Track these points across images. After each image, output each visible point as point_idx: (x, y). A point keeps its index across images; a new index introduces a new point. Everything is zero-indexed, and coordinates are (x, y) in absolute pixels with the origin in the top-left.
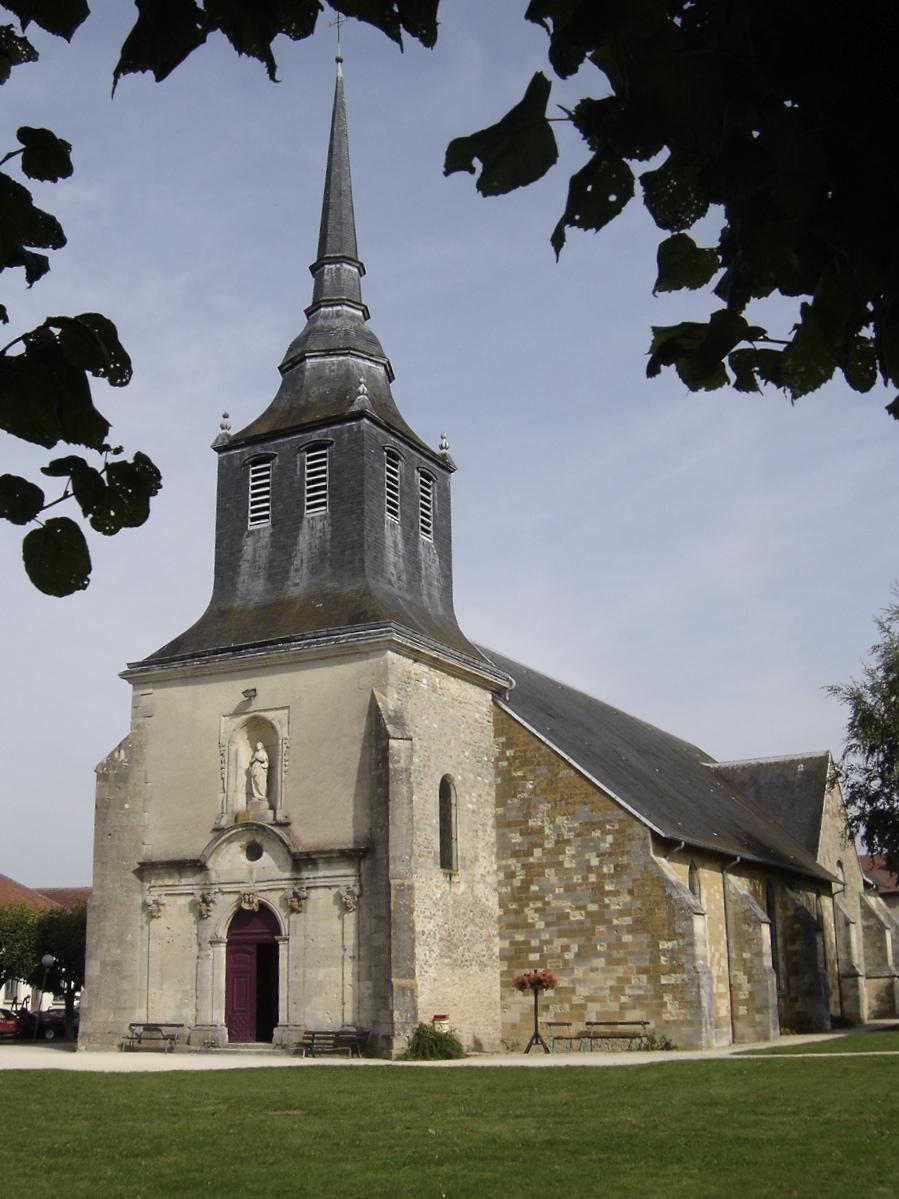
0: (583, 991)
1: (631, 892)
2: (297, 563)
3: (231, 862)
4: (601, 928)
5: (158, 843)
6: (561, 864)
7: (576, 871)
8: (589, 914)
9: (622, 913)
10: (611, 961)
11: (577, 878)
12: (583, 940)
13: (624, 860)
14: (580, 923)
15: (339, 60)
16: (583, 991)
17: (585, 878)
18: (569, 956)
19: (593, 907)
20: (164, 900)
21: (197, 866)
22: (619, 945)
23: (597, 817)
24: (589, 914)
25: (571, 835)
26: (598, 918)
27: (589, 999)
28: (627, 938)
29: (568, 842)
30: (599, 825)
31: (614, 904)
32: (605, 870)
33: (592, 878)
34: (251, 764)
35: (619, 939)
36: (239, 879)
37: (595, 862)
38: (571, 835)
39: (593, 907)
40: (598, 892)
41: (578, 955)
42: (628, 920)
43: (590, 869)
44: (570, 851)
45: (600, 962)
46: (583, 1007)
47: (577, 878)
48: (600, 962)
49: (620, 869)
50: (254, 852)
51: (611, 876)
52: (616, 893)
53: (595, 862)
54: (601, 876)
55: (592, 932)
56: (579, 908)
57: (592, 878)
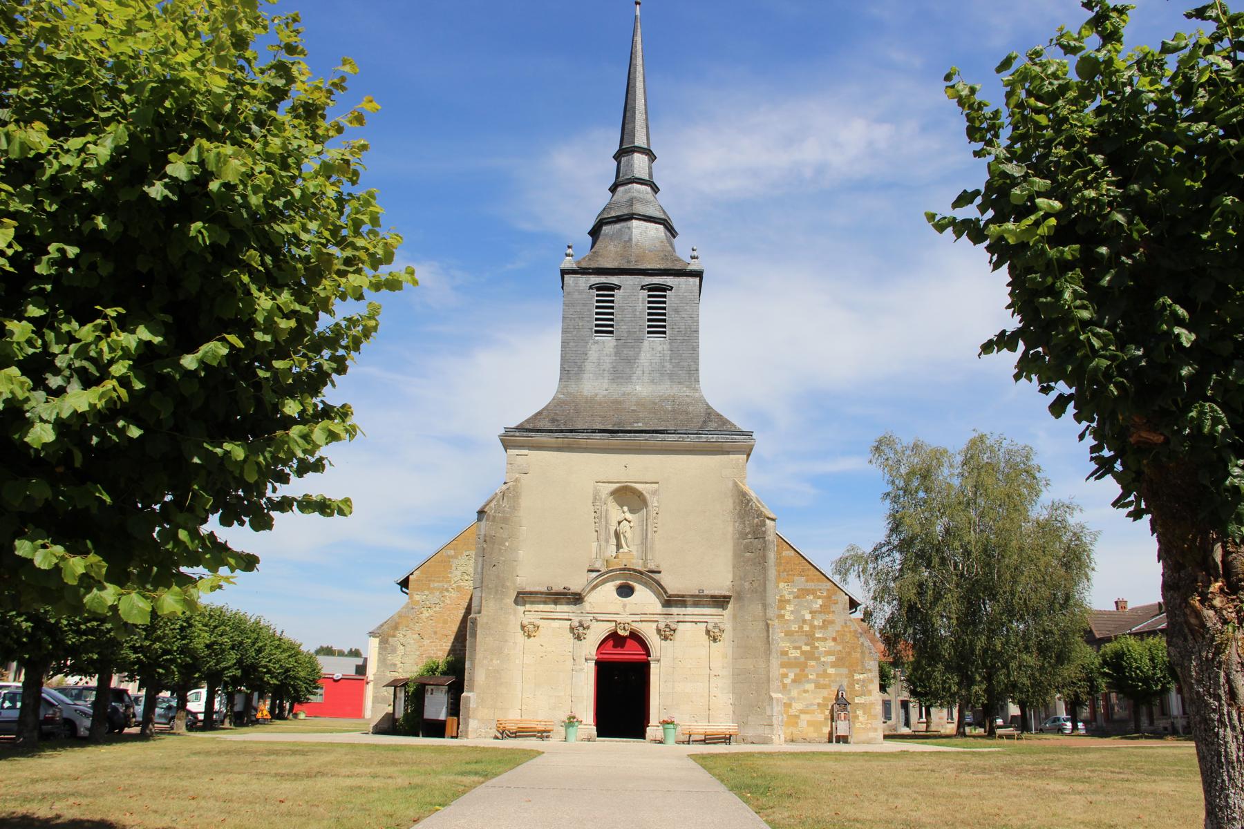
0: (797, 706)
1: (834, 639)
2: (639, 372)
3: (604, 598)
4: (813, 663)
5: (529, 575)
6: (783, 616)
7: (794, 622)
8: (803, 653)
9: (829, 653)
10: (818, 686)
11: (794, 627)
12: (797, 670)
13: (830, 617)
14: (796, 658)
15: (637, 3)
16: (797, 706)
17: (801, 627)
18: (787, 681)
19: (805, 648)
20: (542, 623)
21: (577, 599)
22: (825, 674)
23: (811, 586)
24: (803, 653)
25: (791, 597)
26: (810, 656)
27: (802, 712)
28: (831, 671)
29: (788, 601)
30: (813, 592)
31: (822, 647)
32: (816, 623)
33: (806, 628)
34: (619, 523)
35: (825, 671)
36: (613, 611)
37: (808, 617)
38: (791, 597)
39: (805, 648)
40: (810, 638)
41: (794, 681)
42: (831, 659)
43: (804, 621)
44: (789, 608)
45: (810, 687)
46: (797, 717)
47: (794, 627)
48: (810, 687)
49: (826, 624)
50: (625, 591)
51: (820, 628)
52: (824, 639)
53: (808, 617)
54: (813, 627)
55: (806, 665)
56: (795, 648)
57: (806, 628)
